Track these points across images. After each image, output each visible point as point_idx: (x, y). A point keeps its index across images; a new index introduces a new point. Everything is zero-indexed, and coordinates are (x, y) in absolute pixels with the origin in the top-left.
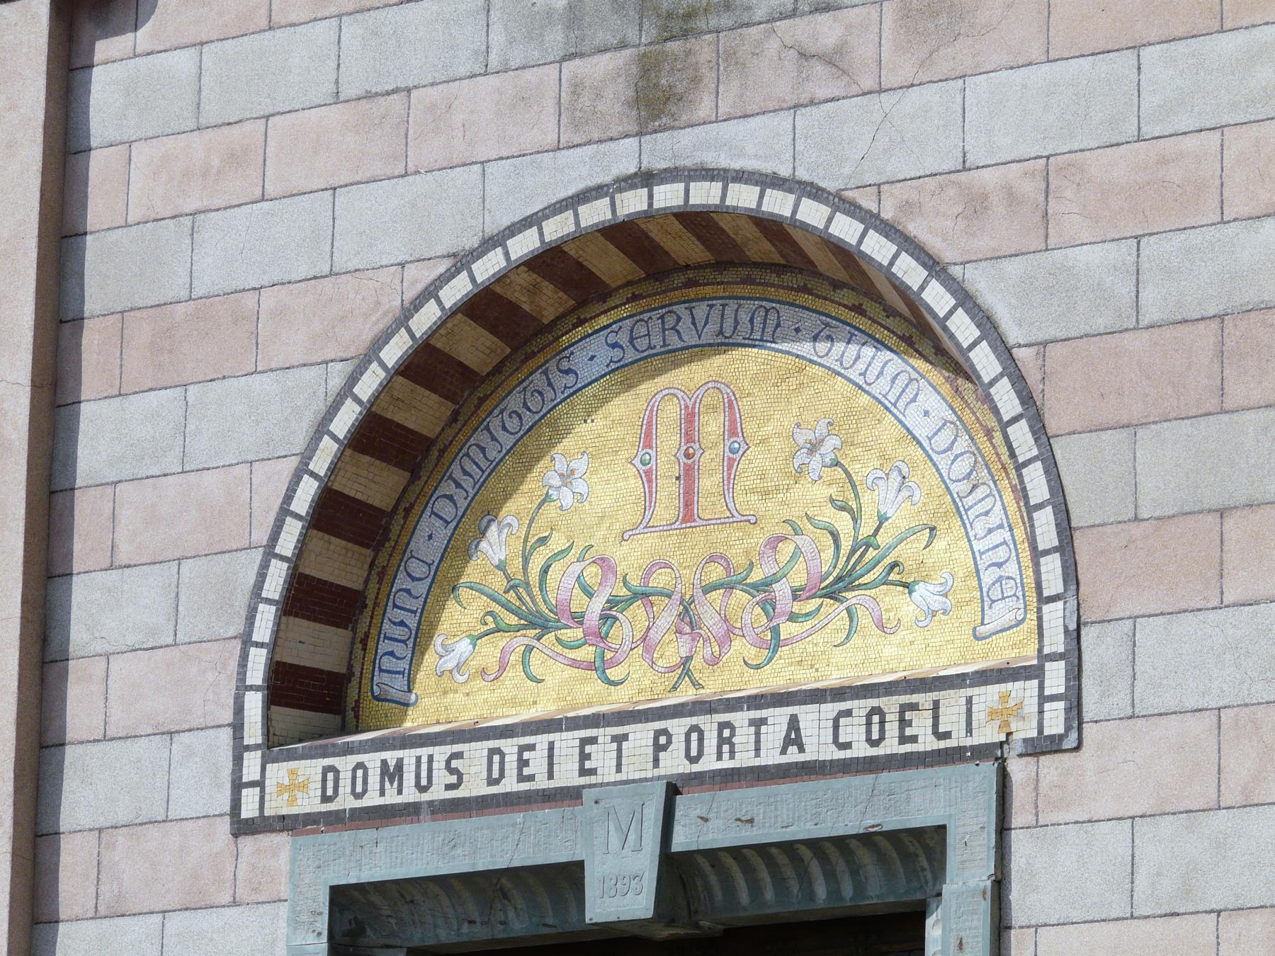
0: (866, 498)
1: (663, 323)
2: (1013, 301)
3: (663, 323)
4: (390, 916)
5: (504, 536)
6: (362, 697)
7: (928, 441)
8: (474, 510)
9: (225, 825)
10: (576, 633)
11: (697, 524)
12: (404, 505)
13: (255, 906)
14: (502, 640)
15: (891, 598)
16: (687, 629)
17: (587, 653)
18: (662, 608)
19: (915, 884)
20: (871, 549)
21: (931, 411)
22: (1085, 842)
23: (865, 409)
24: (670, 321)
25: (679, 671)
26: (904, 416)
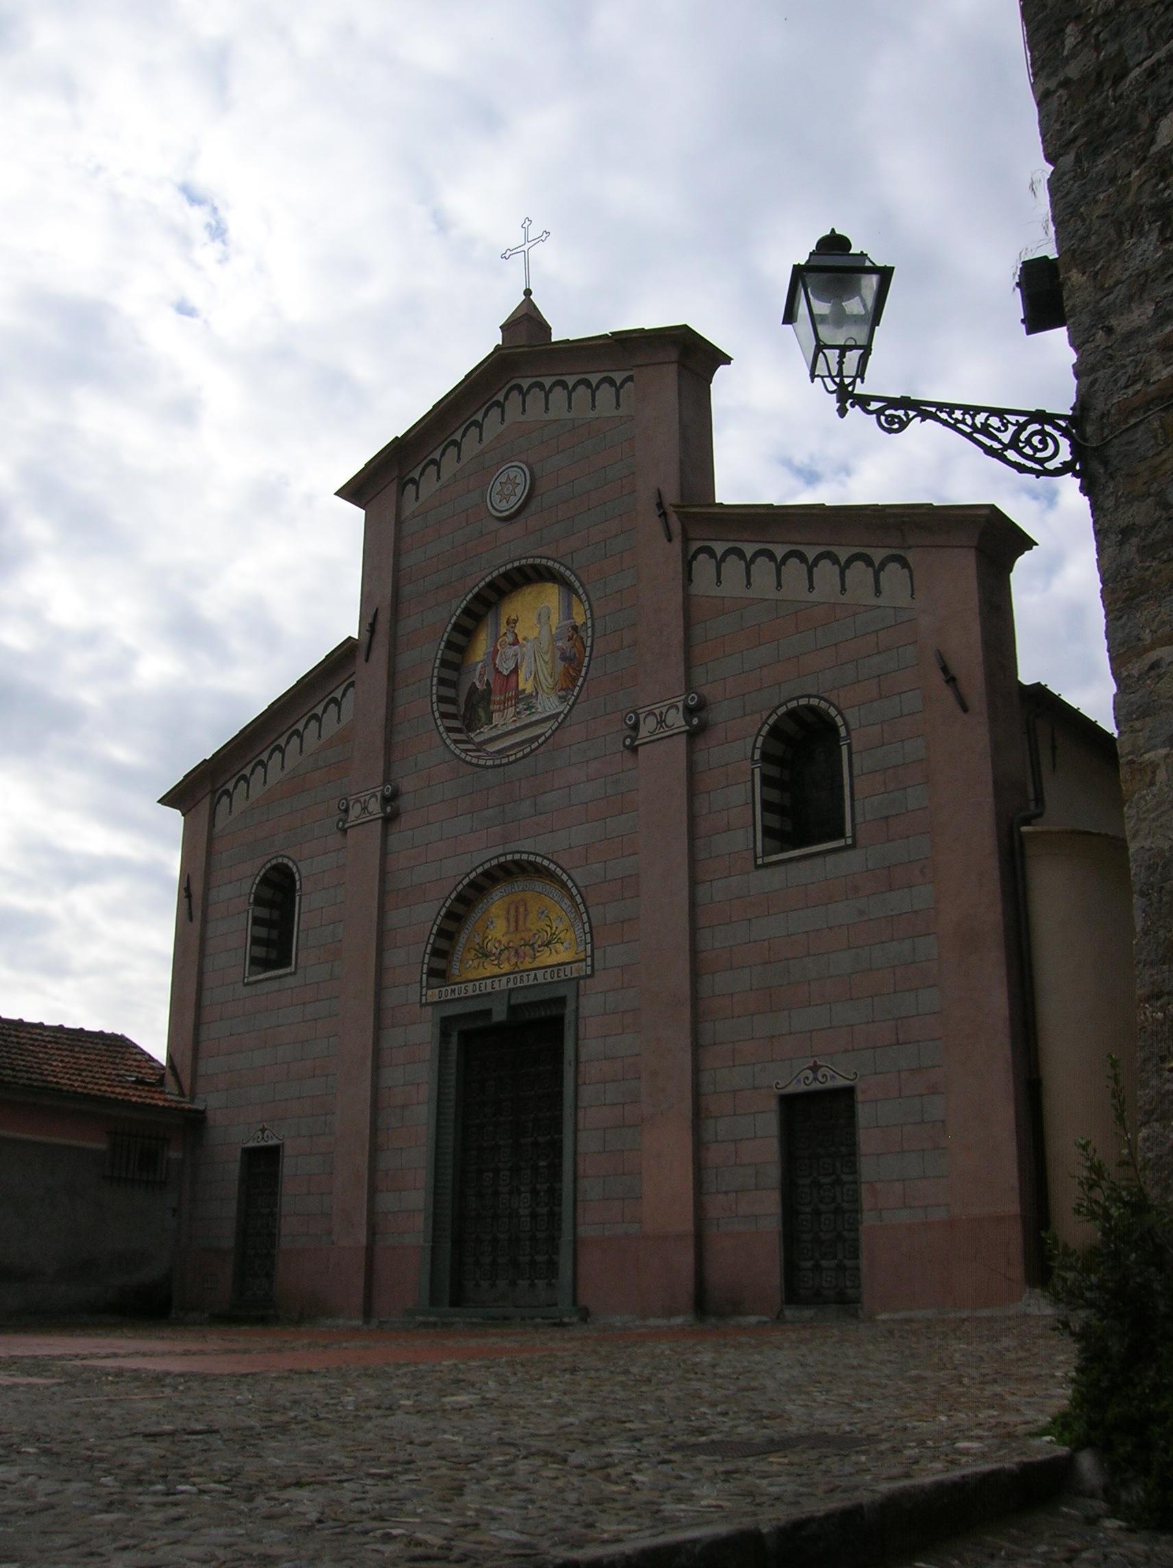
0: (554, 923)
10: (493, 958)
15: (559, 946)
17: (496, 962)
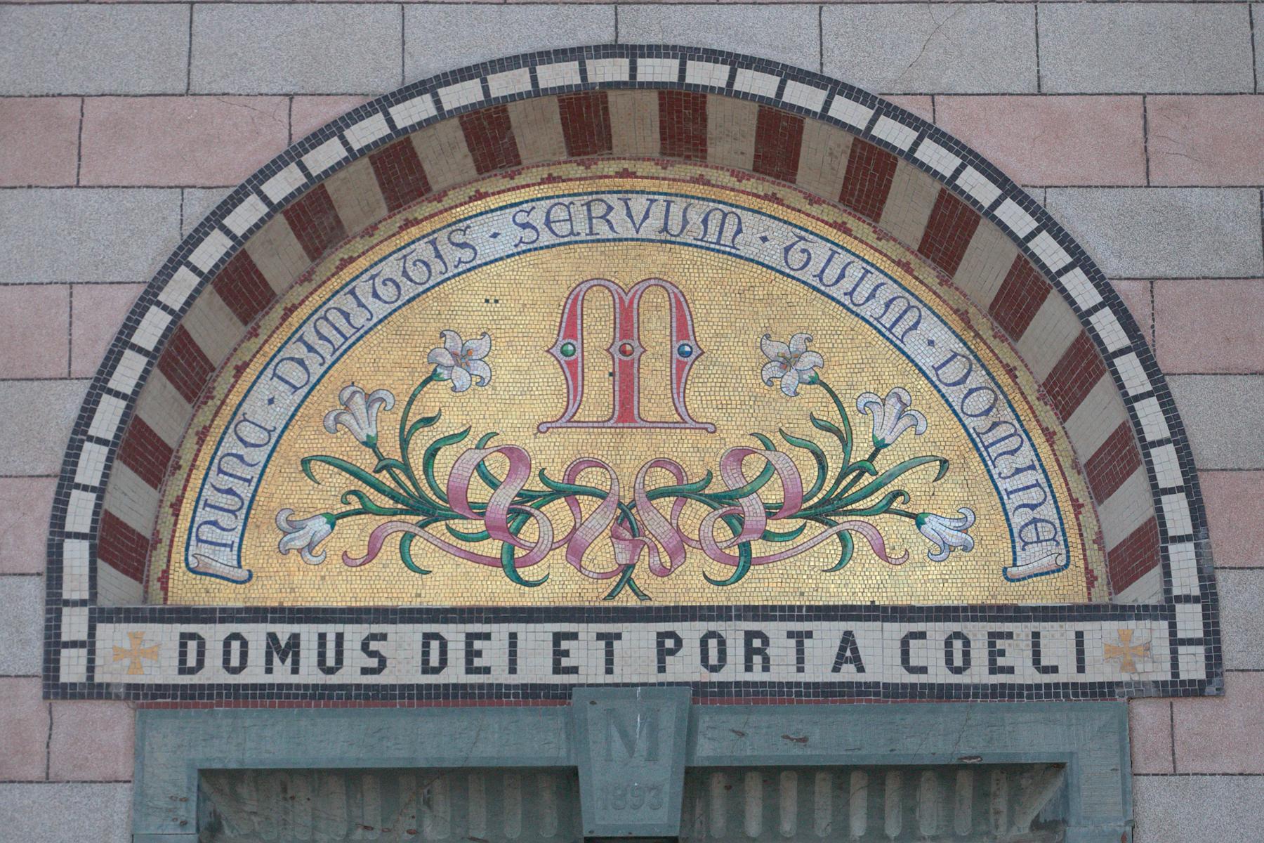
1: (589, 210)
2: (1110, 232)
3: (589, 210)
4: (255, 813)
5: (374, 410)
6: (172, 568)
7: (934, 372)
8: (332, 379)
9: (35, 688)
11: (637, 425)
12: (236, 361)
13: (80, 785)
14: (371, 523)
15: (893, 528)
16: (627, 535)
18: (593, 509)
19: (984, 828)
20: (867, 474)
21: (936, 342)
22: (1237, 795)
23: (852, 330)
24: (598, 210)
25: (618, 579)
26: (902, 342)
